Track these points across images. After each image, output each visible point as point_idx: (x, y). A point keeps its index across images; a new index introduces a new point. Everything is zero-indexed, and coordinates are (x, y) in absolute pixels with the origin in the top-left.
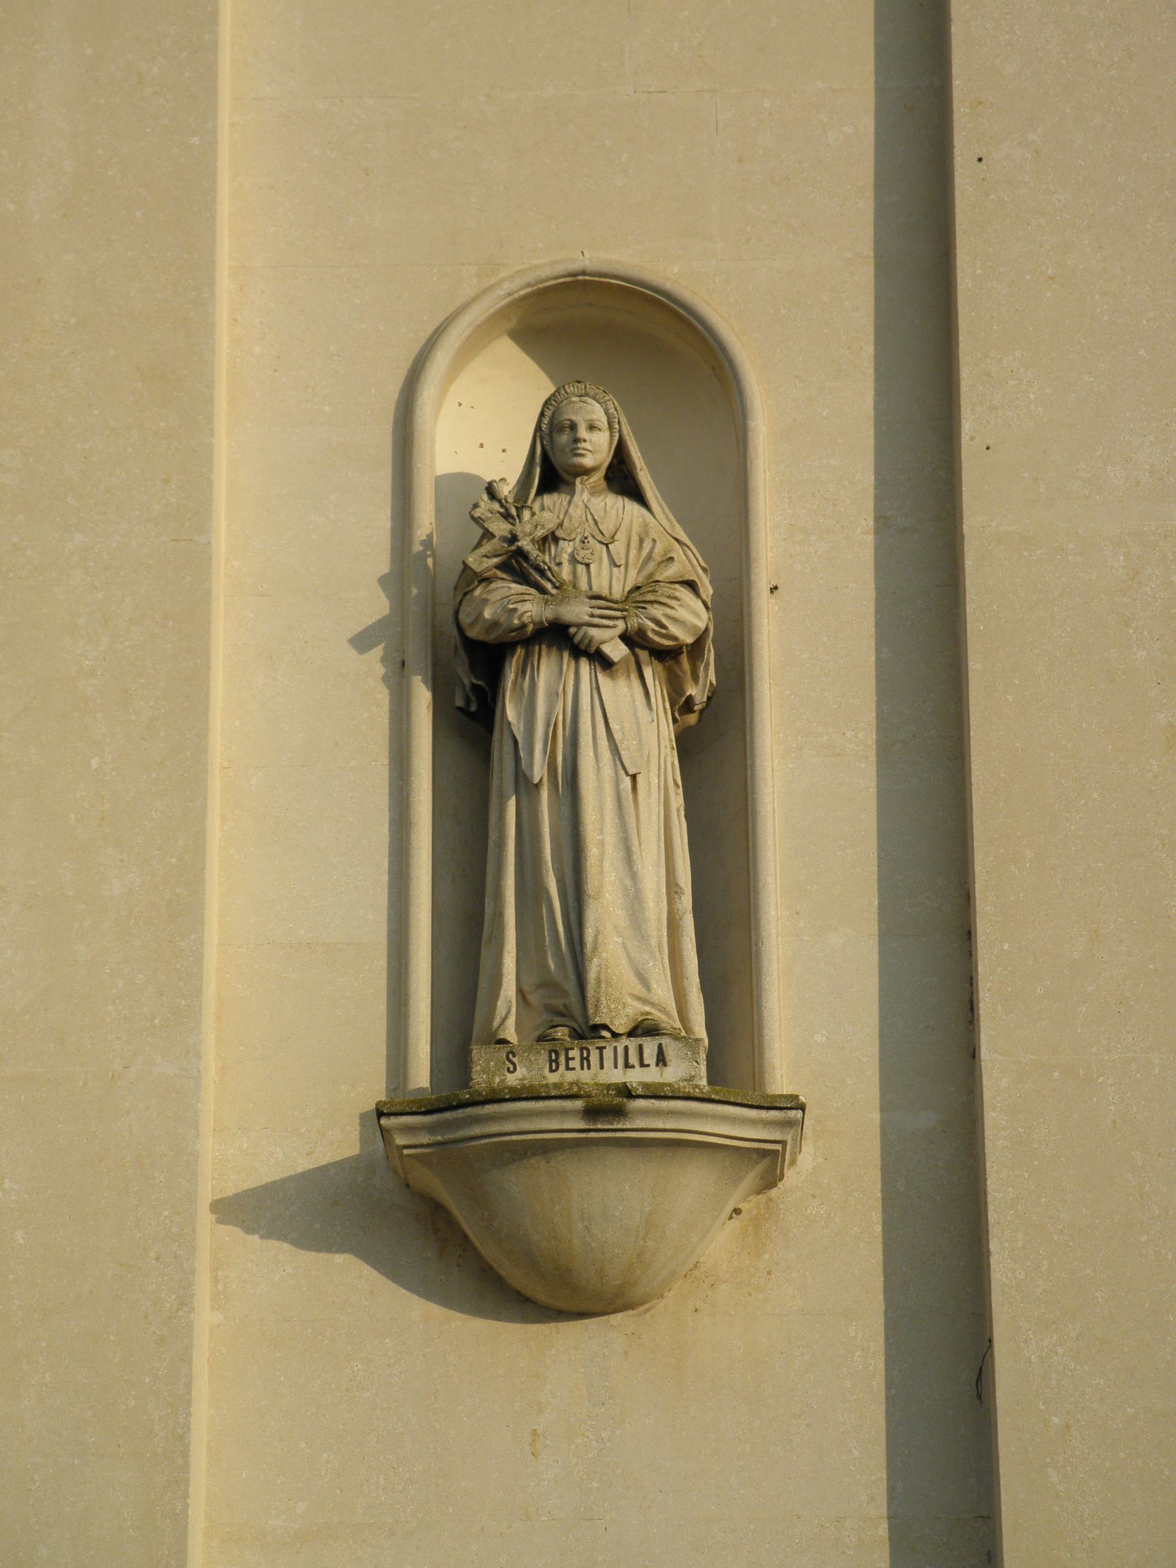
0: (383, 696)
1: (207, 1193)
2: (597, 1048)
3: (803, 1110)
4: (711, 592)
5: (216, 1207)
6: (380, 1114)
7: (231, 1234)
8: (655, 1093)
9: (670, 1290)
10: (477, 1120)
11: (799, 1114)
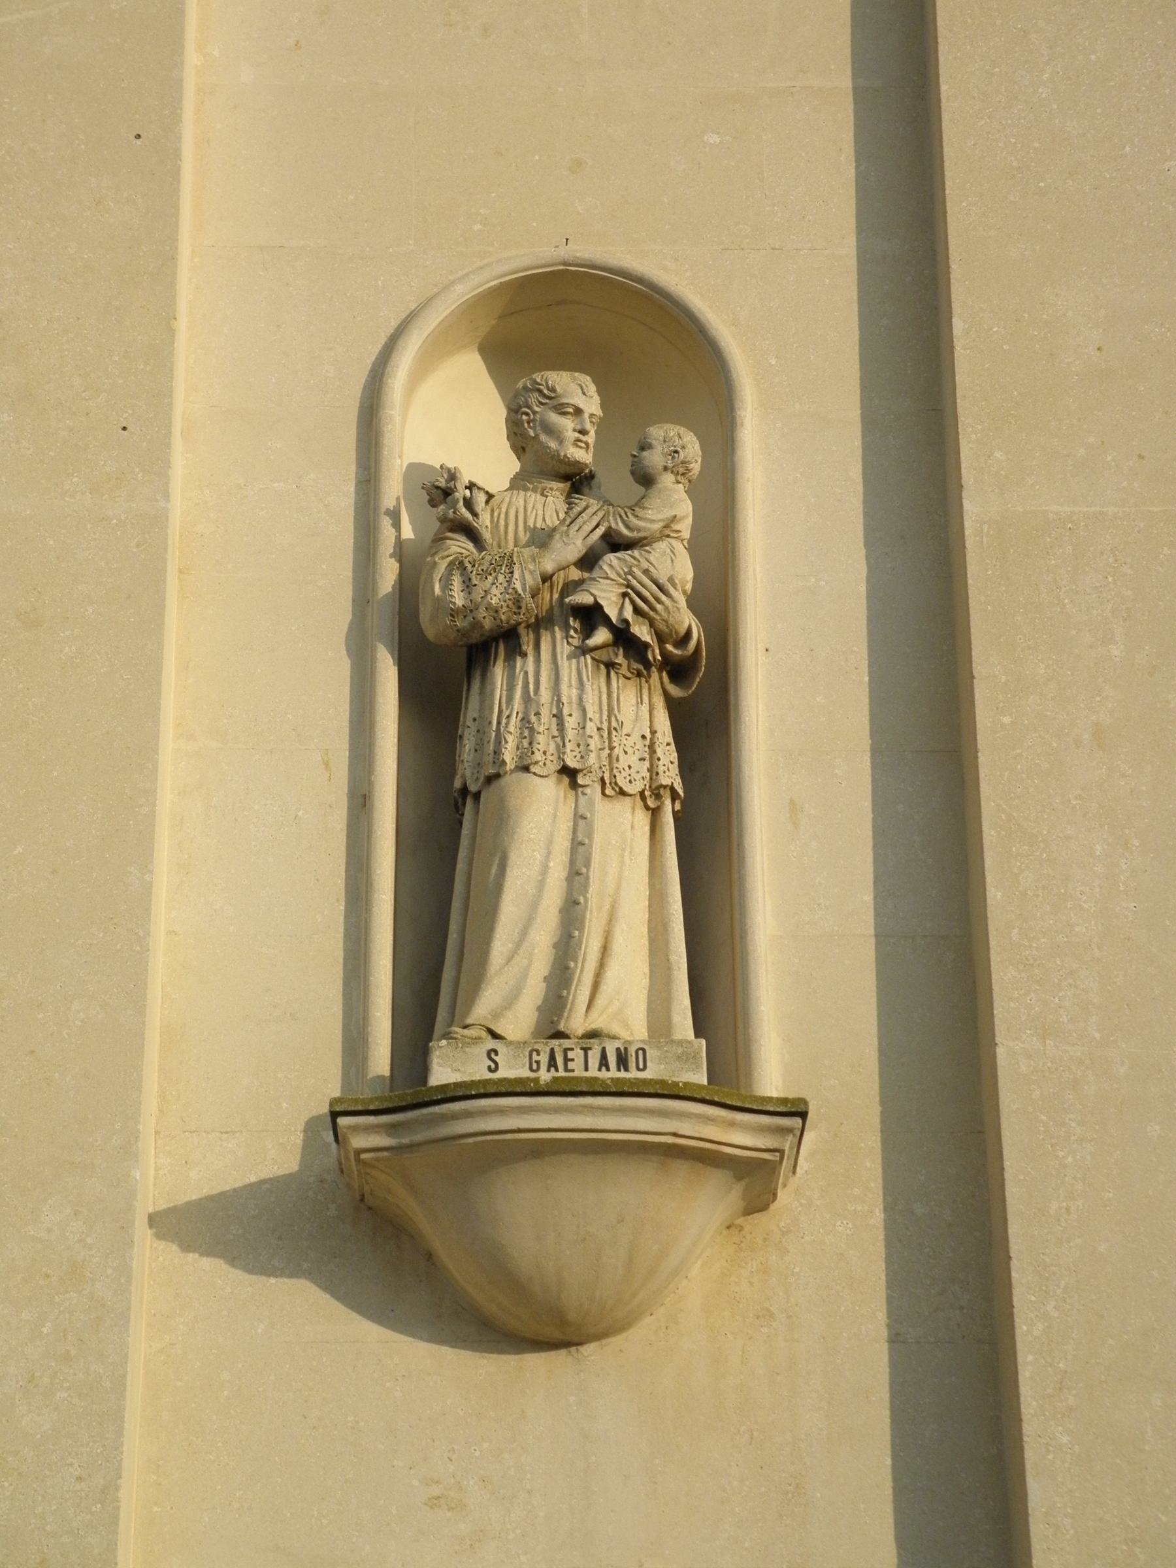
0: (343, 667)
1: (150, 1200)
2: (582, 1049)
3: (803, 1115)
4: (690, 575)
5: (152, 1220)
6: (334, 1115)
7: (170, 1251)
8: (561, 749)
9: (651, 1315)
10: (468, 1114)
11: (799, 1120)
